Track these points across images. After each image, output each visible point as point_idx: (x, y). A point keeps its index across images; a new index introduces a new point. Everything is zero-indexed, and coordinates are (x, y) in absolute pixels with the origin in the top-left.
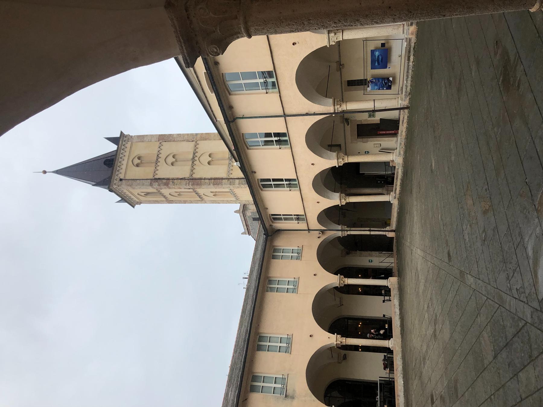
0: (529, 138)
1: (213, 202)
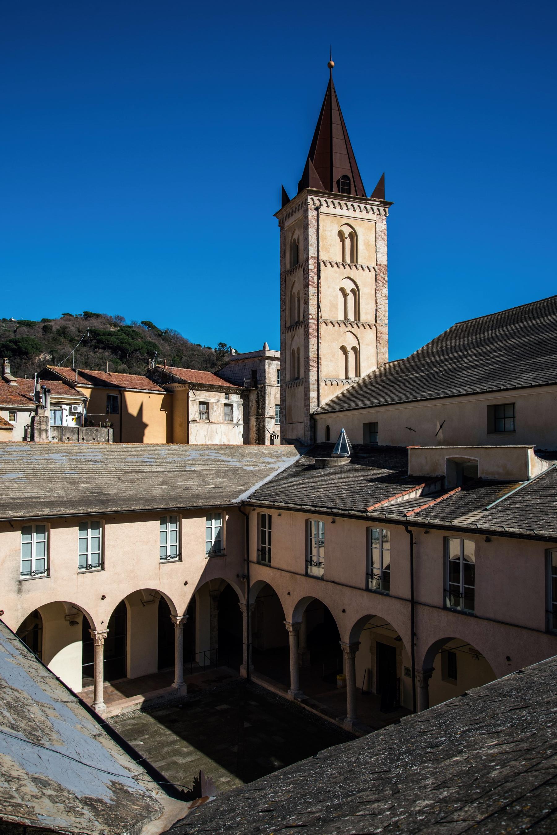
0: (526, 824)
1: (284, 345)
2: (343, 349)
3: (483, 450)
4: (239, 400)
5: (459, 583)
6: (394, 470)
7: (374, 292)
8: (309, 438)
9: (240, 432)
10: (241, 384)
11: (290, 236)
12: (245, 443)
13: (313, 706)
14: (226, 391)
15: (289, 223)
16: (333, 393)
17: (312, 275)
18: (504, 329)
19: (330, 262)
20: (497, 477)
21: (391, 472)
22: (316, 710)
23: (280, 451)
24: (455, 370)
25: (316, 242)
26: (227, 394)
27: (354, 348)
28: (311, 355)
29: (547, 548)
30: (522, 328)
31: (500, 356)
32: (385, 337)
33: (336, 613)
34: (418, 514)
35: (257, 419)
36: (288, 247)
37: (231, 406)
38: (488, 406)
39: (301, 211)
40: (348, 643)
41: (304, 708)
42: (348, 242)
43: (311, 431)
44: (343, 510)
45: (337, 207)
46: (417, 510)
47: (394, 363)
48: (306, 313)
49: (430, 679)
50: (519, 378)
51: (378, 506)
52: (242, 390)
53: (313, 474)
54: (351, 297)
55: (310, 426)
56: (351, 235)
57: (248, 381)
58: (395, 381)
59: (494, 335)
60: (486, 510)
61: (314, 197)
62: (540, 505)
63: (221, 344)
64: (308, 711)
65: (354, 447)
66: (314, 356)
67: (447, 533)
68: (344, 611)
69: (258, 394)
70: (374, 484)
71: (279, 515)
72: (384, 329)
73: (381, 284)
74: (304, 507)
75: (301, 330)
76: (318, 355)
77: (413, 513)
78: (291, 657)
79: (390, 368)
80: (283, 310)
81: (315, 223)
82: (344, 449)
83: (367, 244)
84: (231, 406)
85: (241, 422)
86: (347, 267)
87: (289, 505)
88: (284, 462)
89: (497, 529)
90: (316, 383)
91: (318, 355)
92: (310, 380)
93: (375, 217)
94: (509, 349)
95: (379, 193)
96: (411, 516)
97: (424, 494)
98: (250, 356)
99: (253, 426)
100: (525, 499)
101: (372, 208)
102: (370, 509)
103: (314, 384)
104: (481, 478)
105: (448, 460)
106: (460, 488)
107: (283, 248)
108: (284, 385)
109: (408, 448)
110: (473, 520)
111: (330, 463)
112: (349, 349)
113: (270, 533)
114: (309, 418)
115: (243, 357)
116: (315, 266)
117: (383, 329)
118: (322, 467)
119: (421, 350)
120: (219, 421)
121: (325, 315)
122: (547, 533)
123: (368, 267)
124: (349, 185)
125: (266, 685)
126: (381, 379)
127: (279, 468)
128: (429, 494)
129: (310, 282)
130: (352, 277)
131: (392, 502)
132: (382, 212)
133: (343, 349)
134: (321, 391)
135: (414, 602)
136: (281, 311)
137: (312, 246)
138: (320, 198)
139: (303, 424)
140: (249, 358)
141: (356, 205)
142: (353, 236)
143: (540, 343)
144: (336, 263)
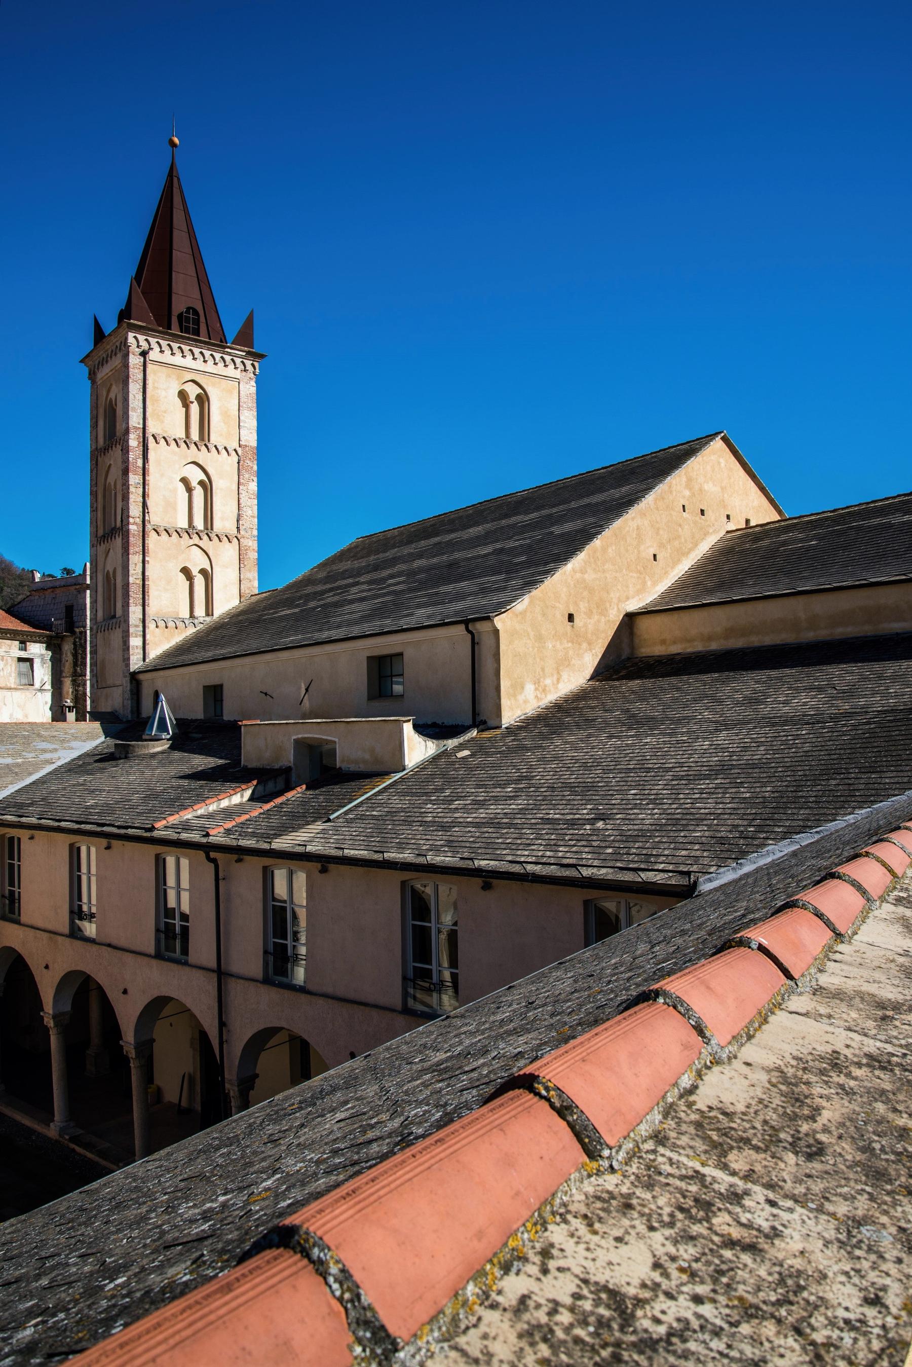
2: (186, 571)
3: (343, 725)
4: (44, 651)
5: (286, 940)
6: (226, 759)
7: (235, 487)
8: (129, 711)
9: (46, 703)
10: (47, 626)
11: (105, 393)
12: (54, 719)
13: (88, 1146)
14: (20, 638)
15: (103, 373)
16: (169, 641)
17: (135, 456)
18: (413, 546)
19: (164, 438)
20: (362, 768)
21: (221, 762)
22: (91, 1152)
23: (73, 731)
24: (336, 605)
25: (141, 405)
26: (23, 642)
27: (203, 572)
28: (131, 580)
29: (404, 879)
30: (435, 545)
31: (399, 583)
32: (254, 555)
33: (114, 995)
34: (228, 832)
35: (74, 682)
36: (101, 411)
37: (30, 661)
38: (368, 658)
39: (119, 355)
40: (133, 1042)
41: (74, 1150)
42: (195, 408)
43: (132, 699)
44: (119, 827)
45: (166, 352)
46: (229, 825)
47: (264, 595)
48: (125, 515)
49: (251, 1092)
50: (412, 615)
51: (173, 819)
52: (47, 636)
53: (105, 769)
54: (198, 493)
55: (131, 691)
56: (199, 398)
57: (59, 622)
58: (258, 621)
59: (399, 554)
60: (329, 820)
61: (139, 336)
62: (407, 810)
63: (65, 569)
64: (80, 1154)
65: (181, 724)
66: (138, 582)
67: (267, 861)
68: (125, 992)
69: (75, 643)
70: (185, 782)
71: (32, 838)
72: (251, 544)
73: (247, 476)
74: (63, 824)
75: (119, 541)
76: (144, 580)
77: (222, 830)
78: (54, 1069)
79: (258, 602)
80: (94, 510)
81: (141, 376)
82: (162, 727)
83: (225, 414)
84: (30, 661)
85: (48, 686)
86: (193, 446)
87: (43, 821)
88: (72, 749)
89: (334, 852)
90: (141, 625)
91: (144, 580)
92: (131, 620)
93: (237, 374)
94: (411, 574)
95: (245, 338)
96: (217, 836)
97: (255, 796)
98: (63, 584)
99: (68, 693)
100: (390, 801)
101: (232, 360)
102: (159, 825)
103: (137, 626)
104: (340, 768)
105: (297, 741)
106: (304, 787)
107: (95, 412)
108: (95, 627)
109: (240, 723)
110: (304, 839)
111: (137, 750)
112: (195, 572)
113: (19, 866)
114: (128, 679)
115: (51, 585)
116: (139, 442)
117: (250, 543)
118: (123, 756)
119: (304, 576)
120: (9, 685)
121: (156, 517)
122: (401, 856)
123: (225, 448)
124: (197, 322)
125: (19, 1117)
126: (240, 618)
127: (59, 758)
128: (264, 796)
129: (131, 466)
130: (201, 463)
131: (200, 812)
132: (249, 367)
133: (186, 571)
134: (148, 637)
135: (221, 974)
136: (92, 511)
137: (134, 410)
138: (149, 338)
139: (121, 688)
140: (60, 587)
141: (207, 353)
142: (203, 399)
143: (451, 565)
144: (175, 440)
